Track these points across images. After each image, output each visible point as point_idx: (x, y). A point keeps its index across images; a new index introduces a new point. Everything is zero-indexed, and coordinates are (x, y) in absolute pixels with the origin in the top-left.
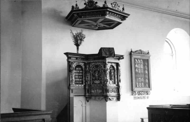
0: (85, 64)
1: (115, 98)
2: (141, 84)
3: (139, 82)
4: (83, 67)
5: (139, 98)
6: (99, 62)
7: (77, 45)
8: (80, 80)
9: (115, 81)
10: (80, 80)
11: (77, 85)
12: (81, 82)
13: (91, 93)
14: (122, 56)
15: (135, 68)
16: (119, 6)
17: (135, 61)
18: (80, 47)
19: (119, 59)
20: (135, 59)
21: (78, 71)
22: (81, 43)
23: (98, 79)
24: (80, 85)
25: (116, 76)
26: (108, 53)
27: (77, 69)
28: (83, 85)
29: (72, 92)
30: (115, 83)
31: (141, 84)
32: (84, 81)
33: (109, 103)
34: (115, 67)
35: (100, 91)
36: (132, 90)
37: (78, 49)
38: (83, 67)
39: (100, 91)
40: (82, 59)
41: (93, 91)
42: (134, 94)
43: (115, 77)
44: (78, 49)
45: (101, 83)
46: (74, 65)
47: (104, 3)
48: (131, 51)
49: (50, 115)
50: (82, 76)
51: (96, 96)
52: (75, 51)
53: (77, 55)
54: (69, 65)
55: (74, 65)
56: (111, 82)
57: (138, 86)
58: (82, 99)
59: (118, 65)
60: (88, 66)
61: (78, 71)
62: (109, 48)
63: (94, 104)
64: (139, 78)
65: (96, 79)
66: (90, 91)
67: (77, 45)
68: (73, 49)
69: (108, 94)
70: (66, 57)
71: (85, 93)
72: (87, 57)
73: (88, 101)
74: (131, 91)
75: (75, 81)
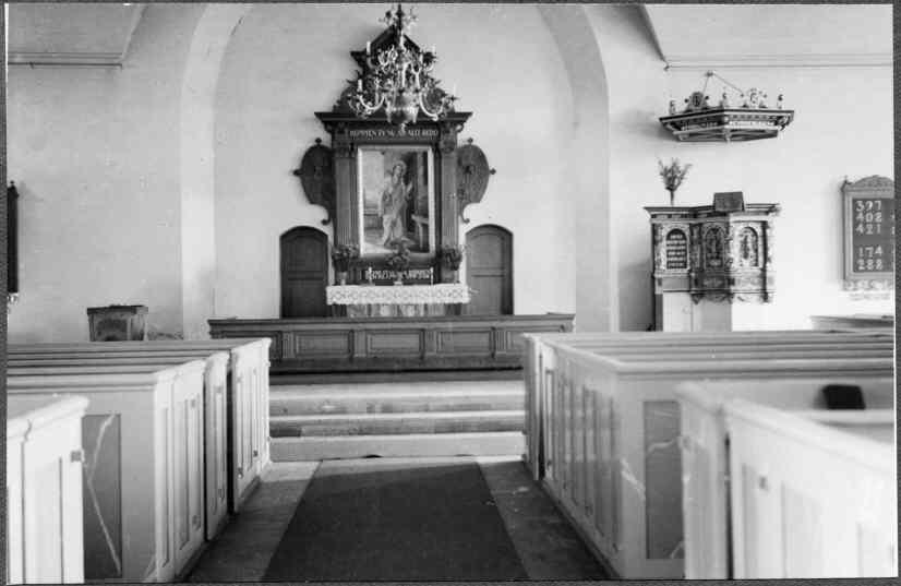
0: (692, 227)
1: (755, 298)
2: (875, 264)
3: (865, 259)
4: (687, 233)
5: (866, 297)
6: (717, 222)
7: (671, 188)
8: (681, 259)
9: (757, 260)
10: (681, 259)
11: (673, 270)
12: (681, 264)
13: (703, 286)
14: (773, 206)
15: (856, 224)
16: (765, 96)
17: (855, 206)
18: (676, 193)
19: (767, 213)
20: (855, 201)
21: (676, 242)
22: (679, 184)
23: (717, 258)
24: (679, 271)
25: (760, 250)
26: (728, 204)
27: (674, 237)
28: (685, 271)
29: (660, 284)
30: (756, 265)
31: (875, 264)
32: (689, 261)
33: (736, 306)
34: (759, 231)
35: (720, 282)
36: (844, 278)
37: (672, 196)
38: (687, 233)
39: (720, 282)
40: (683, 216)
41: (706, 283)
42: (851, 288)
43: (756, 251)
44: (672, 196)
45: (721, 266)
46: (664, 233)
47: (722, 99)
48: (846, 182)
49: (340, 274)
50: (685, 250)
51: (710, 292)
52: (667, 203)
53: (671, 212)
54: (655, 230)
55: (664, 233)
56: (746, 263)
57: (861, 268)
58: (685, 298)
59: (764, 225)
60: (695, 231)
61: (676, 242)
62: (732, 194)
63: (709, 307)
64: (867, 249)
65: (712, 258)
66: (699, 282)
67: (671, 188)
68: (662, 199)
69: (732, 288)
70: (648, 215)
71: (690, 287)
72: (694, 212)
73: (696, 302)
74: (842, 281)
75: (668, 262)
